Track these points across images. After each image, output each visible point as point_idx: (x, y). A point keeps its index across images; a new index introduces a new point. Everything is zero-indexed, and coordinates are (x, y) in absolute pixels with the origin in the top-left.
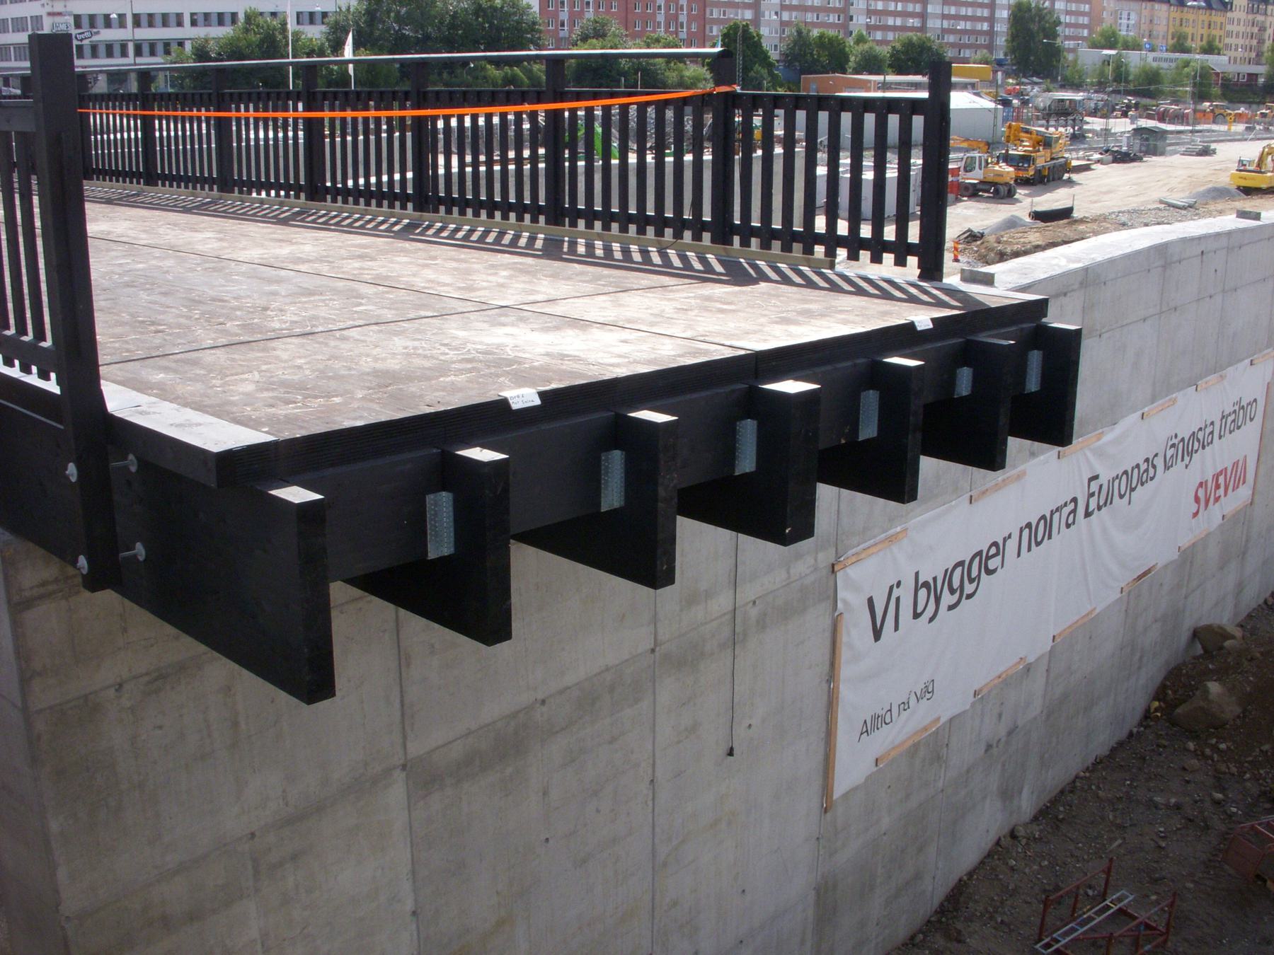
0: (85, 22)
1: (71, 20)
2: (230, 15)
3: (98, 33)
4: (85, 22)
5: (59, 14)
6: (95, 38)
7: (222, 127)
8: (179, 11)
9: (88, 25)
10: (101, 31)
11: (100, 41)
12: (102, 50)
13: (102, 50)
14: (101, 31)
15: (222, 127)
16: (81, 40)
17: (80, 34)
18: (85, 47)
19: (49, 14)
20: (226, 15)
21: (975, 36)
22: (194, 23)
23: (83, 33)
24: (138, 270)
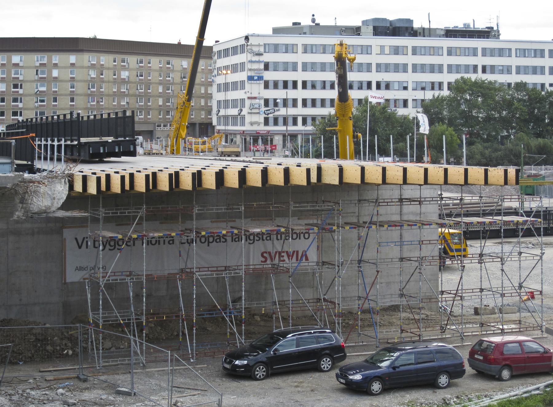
0: (271, 103)
1: (262, 102)
2: (273, 100)
3: (279, 110)
4: (271, 103)
5: (255, 98)
6: (277, 113)
7: (486, 171)
8: (405, 98)
9: (273, 105)
10: (281, 109)
11: (280, 115)
12: (281, 121)
13: (281, 121)
14: (281, 109)
15: (486, 171)
16: (268, 114)
17: (267, 110)
18: (270, 118)
19: (249, 98)
20: (317, 100)
21: (174, 95)
22: (484, 55)
23: (269, 110)
24: (68, 379)
